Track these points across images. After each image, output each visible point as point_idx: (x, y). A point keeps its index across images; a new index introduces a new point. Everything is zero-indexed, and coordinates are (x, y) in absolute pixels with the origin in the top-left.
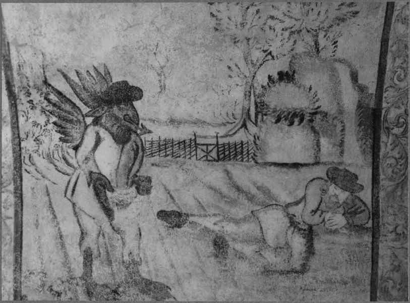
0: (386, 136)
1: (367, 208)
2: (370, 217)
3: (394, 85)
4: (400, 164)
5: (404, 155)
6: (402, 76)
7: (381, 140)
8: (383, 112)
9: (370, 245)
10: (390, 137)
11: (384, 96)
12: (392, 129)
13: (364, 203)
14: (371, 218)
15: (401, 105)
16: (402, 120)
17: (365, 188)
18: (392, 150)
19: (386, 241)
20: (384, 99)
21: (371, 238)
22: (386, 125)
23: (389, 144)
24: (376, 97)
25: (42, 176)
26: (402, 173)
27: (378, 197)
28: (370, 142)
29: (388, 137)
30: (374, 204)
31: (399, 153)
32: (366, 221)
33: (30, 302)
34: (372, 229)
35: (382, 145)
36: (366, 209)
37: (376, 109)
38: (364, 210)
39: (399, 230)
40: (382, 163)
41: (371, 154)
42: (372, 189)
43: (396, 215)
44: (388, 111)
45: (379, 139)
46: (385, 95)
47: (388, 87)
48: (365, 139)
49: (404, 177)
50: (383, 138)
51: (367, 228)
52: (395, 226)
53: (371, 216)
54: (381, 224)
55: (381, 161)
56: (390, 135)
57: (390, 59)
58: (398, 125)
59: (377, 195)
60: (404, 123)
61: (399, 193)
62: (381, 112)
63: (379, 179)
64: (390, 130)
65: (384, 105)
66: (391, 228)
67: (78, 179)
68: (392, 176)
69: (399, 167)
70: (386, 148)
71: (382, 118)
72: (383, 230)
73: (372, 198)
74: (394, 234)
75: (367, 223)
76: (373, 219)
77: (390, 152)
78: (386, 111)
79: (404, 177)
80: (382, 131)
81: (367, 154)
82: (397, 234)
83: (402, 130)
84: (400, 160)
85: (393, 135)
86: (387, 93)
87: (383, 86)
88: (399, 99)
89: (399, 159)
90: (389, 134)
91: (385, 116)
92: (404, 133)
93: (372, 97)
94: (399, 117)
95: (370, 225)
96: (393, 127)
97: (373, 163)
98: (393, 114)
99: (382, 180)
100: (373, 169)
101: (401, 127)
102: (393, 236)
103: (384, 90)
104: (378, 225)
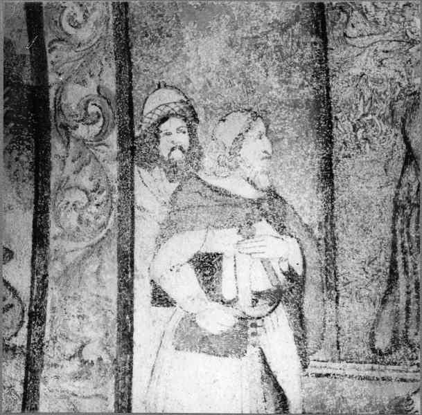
0: (63, 142)
1: (20, 300)
2: (22, 322)
3: (64, 37)
4: (96, 202)
5: (103, 185)
6: (80, 18)
7: (53, 152)
8: (52, 92)
9: (19, 389)
10: (72, 144)
11: (49, 60)
12: (76, 127)
13: (12, 290)
14: (26, 324)
15: (88, 76)
16: (92, 109)
17: (17, 255)
18: (77, 172)
19: (57, 377)
20: (50, 67)
21: (23, 373)
22: (61, 120)
23: (69, 160)
24: (32, 62)
25: (350, 377)
26: (100, 222)
27: (45, 276)
28: (27, 157)
29: (67, 146)
30: (35, 292)
31: (91, 179)
32: (13, 331)
33: (39, 413)
34: (25, 351)
35: (55, 161)
36: (15, 302)
37: (36, 87)
38: (12, 306)
39: (89, 354)
40: (55, 200)
41: (32, 182)
42: (33, 259)
43: (83, 317)
44: (61, 89)
45: (48, 149)
46: (51, 57)
47: (54, 40)
48: (19, 149)
49: (105, 231)
50: (57, 147)
51: (14, 349)
52: (79, 344)
53: (26, 319)
54: (47, 337)
55: (52, 197)
56: (72, 139)
57: (311, 306)
58: (86, 119)
59: (42, 272)
60: (99, 117)
61: (94, 268)
62: (47, 93)
63: (47, 237)
64: (70, 130)
65: (52, 78)
66: (70, 348)
67: (265, 362)
68: (78, 229)
69: (94, 209)
70: (62, 169)
71: (51, 106)
72: (50, 354)
73: (33, 279)
74: (76, 362)
75: (16, 335)
76: (29, 327)
77: (72, 177)
78: (57, 91)
79: (105, 231)
80: (53, 133)
81: (24, 181)
82: (84, 362)
83: (96, 128)
84: (96, 194)
85: (78, 140)
86: (54, 53)
87: (43, 39)
88: (82, 65)
89: (94, 191)
90: (68, 138)
91: (58, 101)
92: (99, 137)
93: (24, 63)
94: (88, 102)
95: (21, 340)
96: (75, 123)
97: (36, 202)
98: (74, 96)
99: (55, 238)
100: (36, 214)
101: (94, 123)
102: (74, 366)
103: (48, 49)
104: (41, 340)
